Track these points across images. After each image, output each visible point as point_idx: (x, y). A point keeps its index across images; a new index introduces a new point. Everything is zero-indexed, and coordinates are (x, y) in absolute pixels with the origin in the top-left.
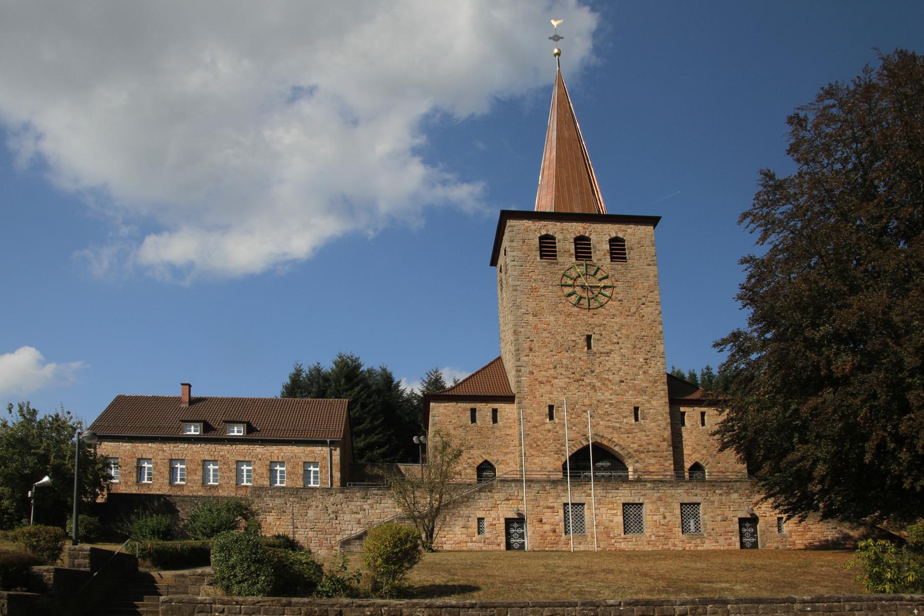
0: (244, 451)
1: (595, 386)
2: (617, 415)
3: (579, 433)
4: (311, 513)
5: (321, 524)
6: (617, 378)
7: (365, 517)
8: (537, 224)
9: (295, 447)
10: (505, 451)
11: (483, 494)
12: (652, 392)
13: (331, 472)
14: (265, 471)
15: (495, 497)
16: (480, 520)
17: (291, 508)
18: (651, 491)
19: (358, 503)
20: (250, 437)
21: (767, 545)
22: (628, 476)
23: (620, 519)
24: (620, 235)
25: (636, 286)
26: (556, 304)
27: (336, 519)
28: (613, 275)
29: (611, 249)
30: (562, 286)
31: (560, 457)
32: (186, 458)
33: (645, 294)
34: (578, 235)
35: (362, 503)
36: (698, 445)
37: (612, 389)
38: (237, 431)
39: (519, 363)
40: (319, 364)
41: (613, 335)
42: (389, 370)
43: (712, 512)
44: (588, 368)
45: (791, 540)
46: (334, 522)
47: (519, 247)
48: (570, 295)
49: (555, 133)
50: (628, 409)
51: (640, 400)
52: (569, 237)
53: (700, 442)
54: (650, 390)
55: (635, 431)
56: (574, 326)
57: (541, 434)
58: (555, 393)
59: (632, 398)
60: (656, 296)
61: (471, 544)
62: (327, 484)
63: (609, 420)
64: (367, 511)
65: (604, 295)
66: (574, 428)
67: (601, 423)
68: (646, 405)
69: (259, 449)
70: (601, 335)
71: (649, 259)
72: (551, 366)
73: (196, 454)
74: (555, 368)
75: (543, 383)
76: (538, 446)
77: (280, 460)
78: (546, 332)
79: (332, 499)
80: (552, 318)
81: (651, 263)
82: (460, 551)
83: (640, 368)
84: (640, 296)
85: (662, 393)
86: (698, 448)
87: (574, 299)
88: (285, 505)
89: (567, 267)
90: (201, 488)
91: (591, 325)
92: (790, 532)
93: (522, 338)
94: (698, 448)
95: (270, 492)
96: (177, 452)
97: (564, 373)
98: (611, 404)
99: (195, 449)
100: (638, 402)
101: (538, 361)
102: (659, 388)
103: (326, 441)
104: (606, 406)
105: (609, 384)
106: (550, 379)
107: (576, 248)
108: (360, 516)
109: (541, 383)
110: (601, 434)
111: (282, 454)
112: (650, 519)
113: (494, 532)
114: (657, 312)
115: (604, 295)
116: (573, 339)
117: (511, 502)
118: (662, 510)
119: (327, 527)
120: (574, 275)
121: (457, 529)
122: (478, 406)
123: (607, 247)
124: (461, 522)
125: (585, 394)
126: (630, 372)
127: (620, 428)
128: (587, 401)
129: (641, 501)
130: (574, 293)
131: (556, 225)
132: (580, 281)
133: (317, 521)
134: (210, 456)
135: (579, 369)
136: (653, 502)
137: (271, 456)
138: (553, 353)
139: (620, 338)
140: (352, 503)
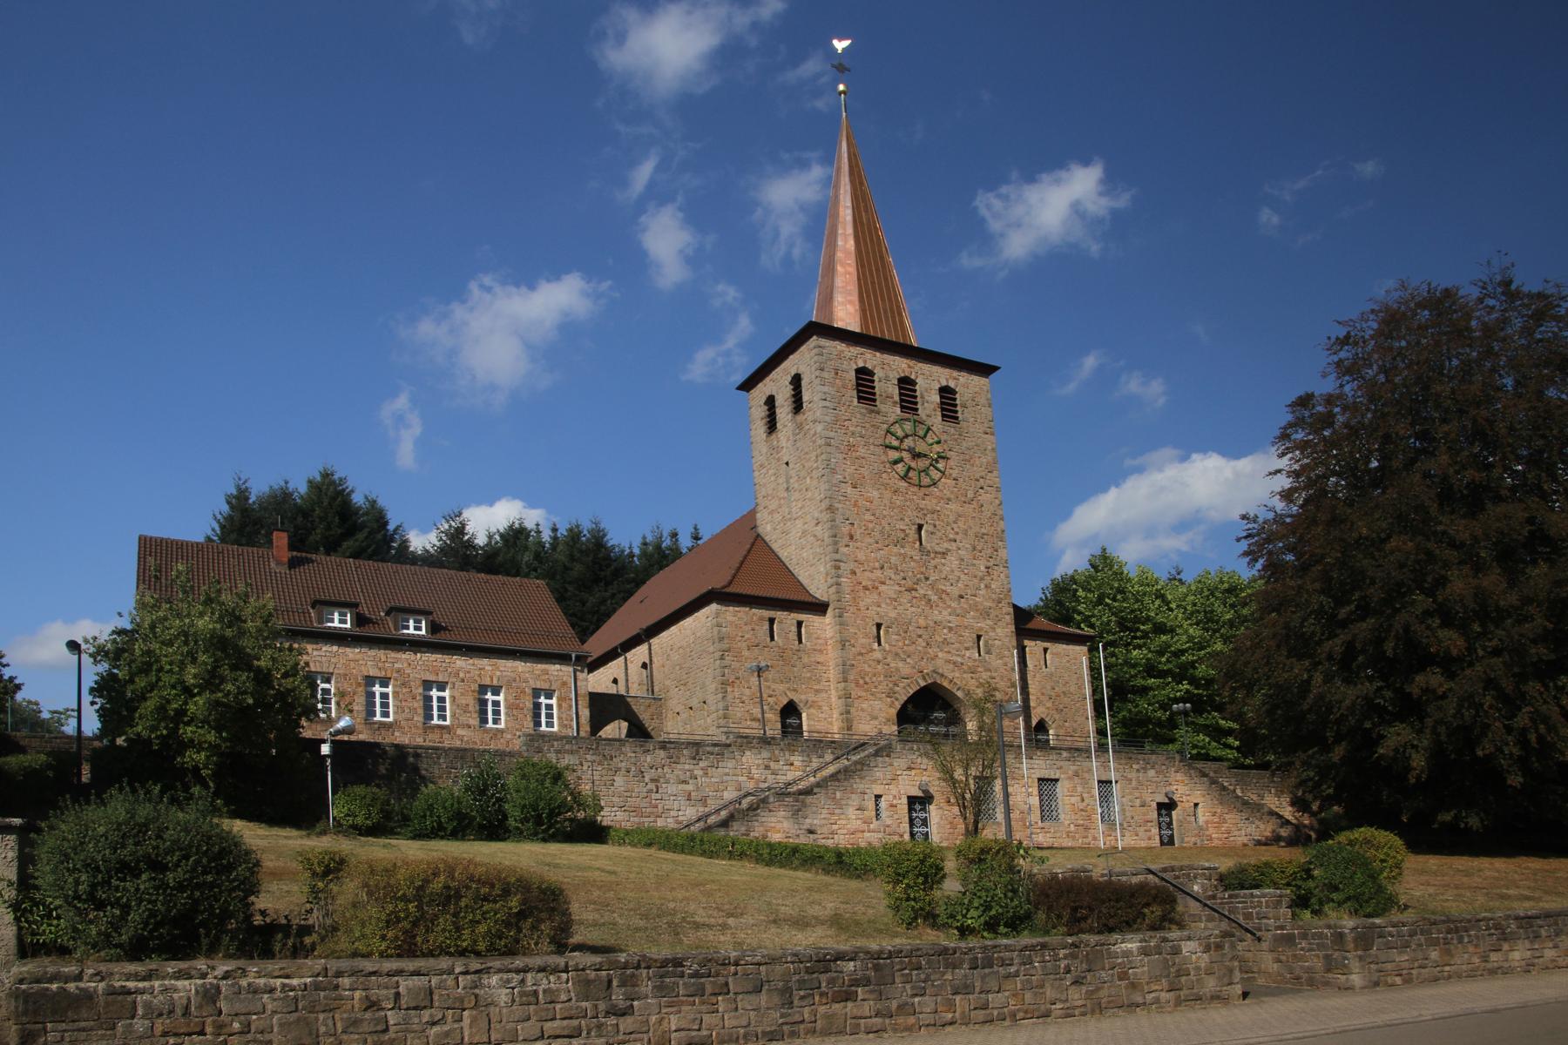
0: (434, 664)
1: (930, 600)
2: (957, 645)
3: (914, 668)
4: (619, 780)
5: (634, 799)
6: (955, 591)
7: (698, 789)
8: (852, 349)
9: (517, 663)
10: (815, 687)
11: (880, 759)
12: (997, 616)
13: (577, 709)
14: (471, 701)
15: (895, 764)
16: (878, 797)
17: (590, 772)
18: (1067, 763)
19: (687, 767)
20: (436, 639)
21: (1186, 839)
22: (1048, 741)
23: (1035, 801)
24: (952, 384)
25: (972, 461)
26: (880, 473)
27: (657, 792)
28: (945, 441)
29: (942, 403)
30: (887, 447)
31: (893, 702)
32: (336, 671)
33: (983, 474)
34: (903, 375)
35: (692, 767)
36: (1043, 694)
37: (950, 606)
38: (415, 628)
39: (837, 557)
40: (286, 483)
41: (949, 528)
42: (381, 502)
43: (1131, 794)
44: (922, 573)
45: (1207, 833)
46: (654, 796)
47: (831, 380)
48: (896, 462)
49: (849, 211)
50: (969, 637)
51: (984, 625)
52: (891, 376)
53: (1044, 691)
54: (993, 613)
55: (980, 669)
56: (902, 508)
57: (870, 666)
58: (883, 606)
59: (975, 623)
60: (993, 478)
61: (869, 834)
62: (571, 727)
63: (949, 652)
64: (699, 779)
65: (937, 469)
66: (908, 660)
67: (940, 655)
68: (991, 634)
69: (460, 662)
70: (935, 526)
71: (986, 425)
72: (877, 565)
73: (352, 665)
74: (882, 568)
75: (868, 589)
76: (866, 683)
77: (495, 682)
78: (869, 513)
79: (649, 759)
80: (875, 494)
81: (988, 430)
82: (1062, 849)
83: (982, 579)
84: (977, 476)
85: (1008, 617)
86: (1042, 698)
87: (900, 468)
88: (580, 767)
89: (892, 420)
90: (363, 726)
91: (922, 509)
92: (1207, 822)
93: (839, 519)
94: (1042, 698)
95: (555, 743)
96: (319, 659)
97: (893, 577)
98: (951, 629)
99: (351, 656)
100: (981, 629)
101: (861, 556)
102: (1004, 610)
103: (571, 656)
104: (945, 631)
105: (947, 599)
106: (876, 584)
107: (901, 394)
108: (690, 787)
109: (866, 588)
110: (940, 671)
111: (498, 673)
112: (1068, 802)
113: (896, 816)
114: (997, 502)
115: (937, 469)
116: (902, 527)
117: (913, 772)
118: (1079, 789)
119: (645, 805)
120: (900, 433)
121: (851, 812)
122: (779, 615)
123: (937, 398)
124: (855, 800)
125: (919, 610)
126: (971, 583)
127: (962, 664)
128: (922, 622)
129: (1057, 777)
130: (901, 460)
131: (875, 356)
132: (908, 442)
133: (629, 794)
134: (377, 670)
135: (910, 574)
136: (1069, 778)
137: (480, 676)
138: (879, 546)
139: (957, 533)
140: (679, 766)
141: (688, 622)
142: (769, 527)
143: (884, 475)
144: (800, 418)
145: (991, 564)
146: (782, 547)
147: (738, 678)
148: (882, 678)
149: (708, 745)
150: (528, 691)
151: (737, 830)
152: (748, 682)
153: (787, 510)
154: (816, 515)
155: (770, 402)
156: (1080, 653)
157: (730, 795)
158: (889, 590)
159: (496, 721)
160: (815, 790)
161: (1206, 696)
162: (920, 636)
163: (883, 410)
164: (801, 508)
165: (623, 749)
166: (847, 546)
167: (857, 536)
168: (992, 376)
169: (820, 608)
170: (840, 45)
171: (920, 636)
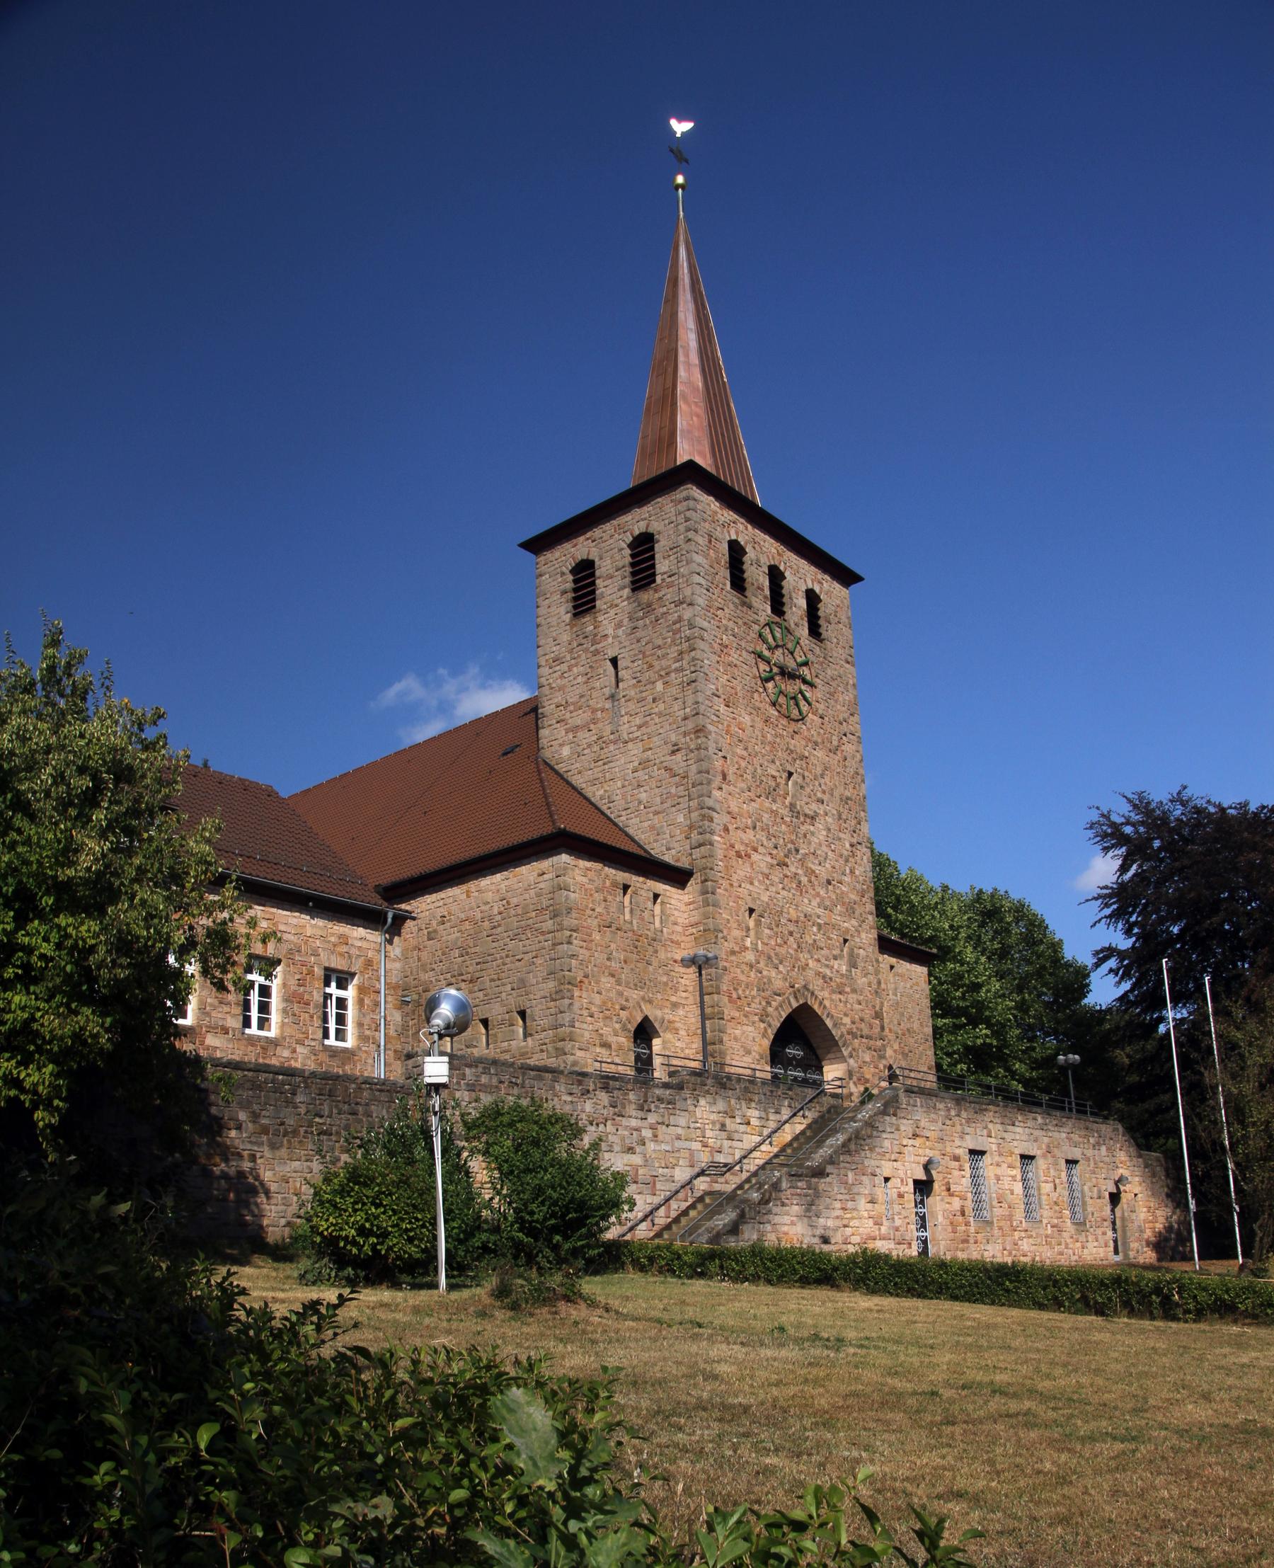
11: (887, 1118)
58: (756, 883)
70: (804, 778)
91: (792, 752)
95: (468, 1071)
100: (847, 930)
101: (734, 805)
109: (739, 855)
127: (831, 979)
128: (793, 914)
140: (624, 1122)
141: (492, 885)
142: (566, 751)
143: (756, 695)
144: (645, 596)
145: (855, 841)
146: (593, 782)
147: (586, 976)
148: (754, 992)
149: (657, 1086)
150: (319, 972)
151: (749, 1235)
152: (598, 982)
153: (608, 729)
154: (673, 738)
155: (584, 572)
156: (921, 971)
157: (682, 1174)
158: (761, 860)
159: (263, 1023)
160: (829, 1169)
161: (995, 1047)
162: (791, 934)
163: (755, 604)
164: (640, 727)
165: (557, 1087)
166: (720, 788)
167: (731, 777)
168: (853, 587)
169: (679, 877)
170: (680, 127)
171: (791, 934)
